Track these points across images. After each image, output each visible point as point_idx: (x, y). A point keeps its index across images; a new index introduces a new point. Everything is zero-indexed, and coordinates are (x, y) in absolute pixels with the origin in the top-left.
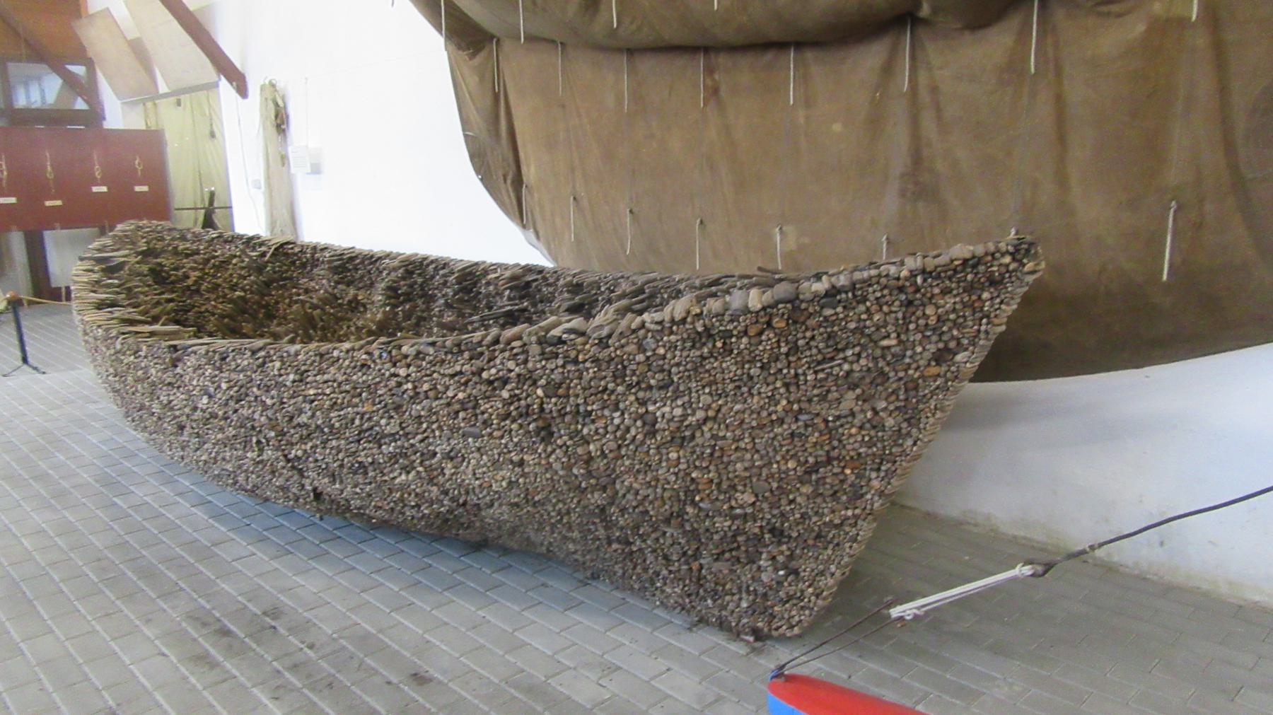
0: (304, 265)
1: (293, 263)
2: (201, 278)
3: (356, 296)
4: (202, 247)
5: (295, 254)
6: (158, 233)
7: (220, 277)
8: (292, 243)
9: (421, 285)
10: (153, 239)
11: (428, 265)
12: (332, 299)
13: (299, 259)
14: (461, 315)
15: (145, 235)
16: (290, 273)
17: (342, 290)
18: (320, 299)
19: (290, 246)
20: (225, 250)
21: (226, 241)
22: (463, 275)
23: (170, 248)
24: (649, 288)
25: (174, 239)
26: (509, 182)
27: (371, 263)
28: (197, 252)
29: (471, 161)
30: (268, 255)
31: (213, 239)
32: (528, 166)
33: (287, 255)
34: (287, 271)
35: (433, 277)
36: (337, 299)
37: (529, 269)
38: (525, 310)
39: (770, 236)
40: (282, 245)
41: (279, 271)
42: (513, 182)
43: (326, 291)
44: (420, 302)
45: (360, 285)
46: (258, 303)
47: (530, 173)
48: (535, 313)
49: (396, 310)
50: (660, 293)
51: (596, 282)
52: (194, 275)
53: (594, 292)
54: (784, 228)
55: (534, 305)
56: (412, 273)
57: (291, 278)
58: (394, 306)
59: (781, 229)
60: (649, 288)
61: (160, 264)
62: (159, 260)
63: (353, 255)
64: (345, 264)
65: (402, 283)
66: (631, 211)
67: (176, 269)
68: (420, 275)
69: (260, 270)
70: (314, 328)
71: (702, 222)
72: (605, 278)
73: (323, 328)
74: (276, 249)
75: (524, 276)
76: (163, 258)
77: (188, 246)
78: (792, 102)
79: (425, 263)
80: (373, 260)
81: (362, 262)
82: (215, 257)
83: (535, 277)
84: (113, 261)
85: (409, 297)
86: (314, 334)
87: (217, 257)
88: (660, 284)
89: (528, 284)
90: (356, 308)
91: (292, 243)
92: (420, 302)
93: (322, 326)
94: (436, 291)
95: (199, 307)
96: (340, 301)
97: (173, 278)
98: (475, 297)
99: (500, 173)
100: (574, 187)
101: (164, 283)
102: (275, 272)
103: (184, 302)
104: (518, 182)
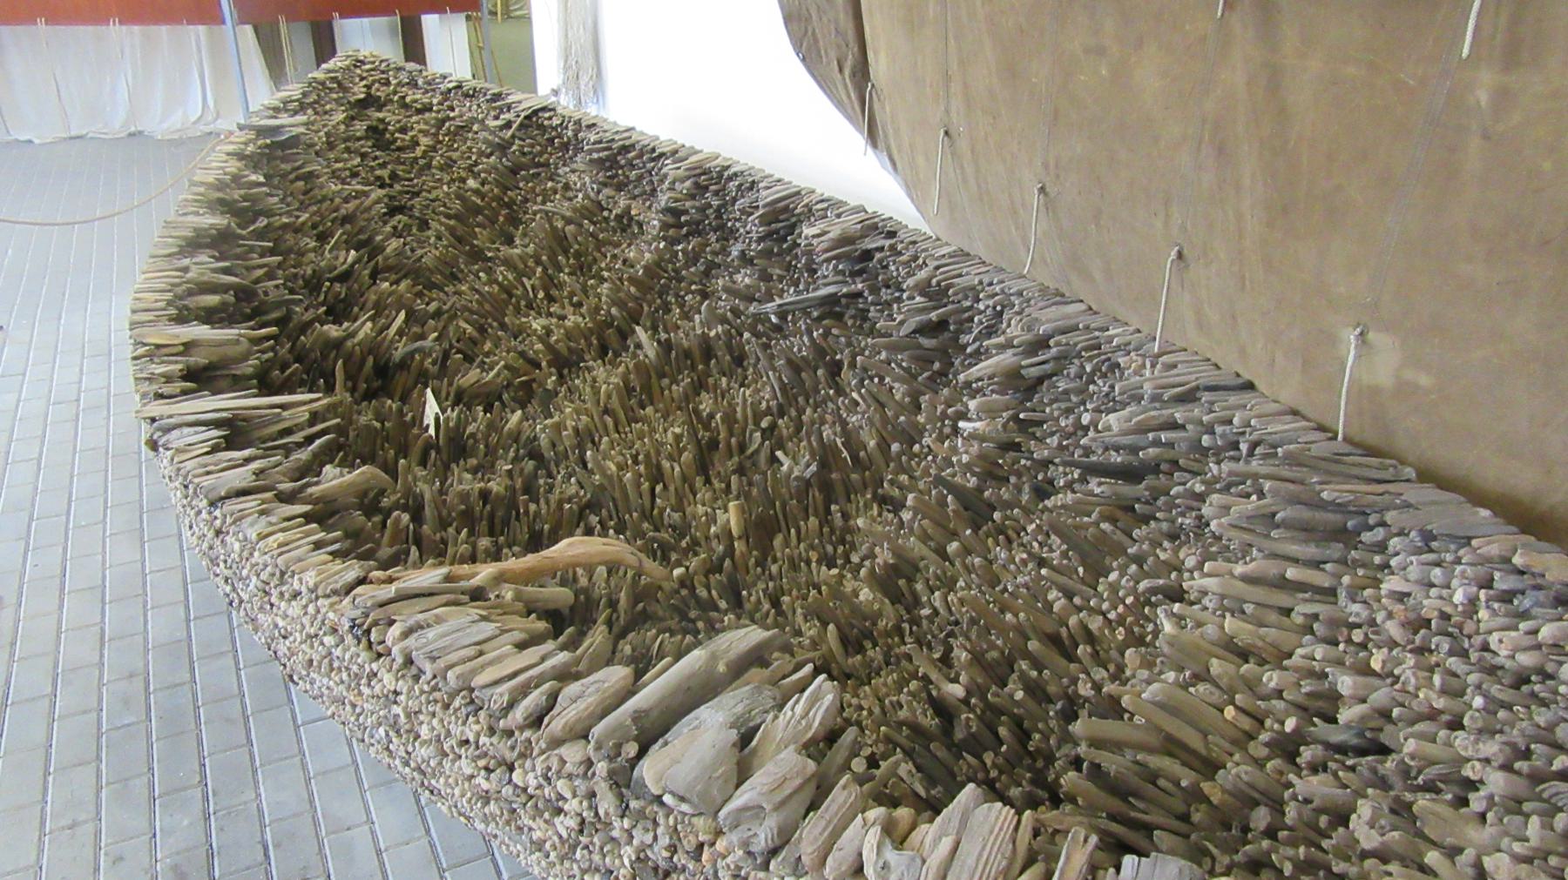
0: (565, 147)
1: (551, 141)
2: (434, 149)
3: (629, 208)
4: (435, 101)
5: (555, 129)
6: (383, 72)
7: (457, 149)
8: (550, 110)
9: (718, 210)
10: (374, 82)
11: (730, 179)
12: (595, 210)
13: (560, 136)
14: (765, 277)
15: (365, 74)
16: (546, 156)
17: (609, 197)
18: (575, 210)
19: (547, 115)
20: (464, 109)
21: (466, 95)
22: (774, 211)
23: (396, 98)
24: (1058, 344)
25: (400, 84)
26: (847, 72)
27: (653, 160)
28: (428, 108)
29: (786, 27)
30: (515, 126)
31: (449, 91)
32: (876, 53)
33: (541, 127)
34: (541, 154)
35: (734, 200)
36: (603, 209)
37: (874, 226)
38: (859, 294)
39: (1332, 340)
40: (535, 112)
41: (530, 153)
42: (853, 75)
43: (586, 196)
44: (713, 237)
45: (636, 192)
46: (499, 199)
47: (879, 66)
48: (873, 303)
49: (676, 248)
50: (1079, 356)
51: (973, 288)
52: (425, 141)
53: (967, 304)
54: (1371, 336)
55: (874, 290)
56: (706, 188)
57: (546, 165)
58: (673, 242)
59: (1361, 334)
60: (1058, 344)
61: (382, 121)
62: (381, 115)
63: (627, 143)
64: (615, 155)
65: (688, 204)
66: (1042, 190)
67: (403, 130)
68: (716, 193)
69: (503, 148)
70: (566, 252)
71: (1180, 255)
72: (991, 284)
73: (578, 255)
74: (526, 117)
75: (863, 236)
76: (389, 111)
77: (418, 96)
78: (1465, 52)
79: (726, 174)
80: (654, 155)
81: (640, 156)
82: (449, 119)
83: (879, 244)
84: (282, 134)
85: (696, 229)
86: (564, 261)
87: (453, 119)
88: (1078, 339)
89: (867, 255)
90: (629, 226)
91: (550, 110)
92: (713, 237)
93: (576, 251)
94: (738, 224)
95: (429, 192)
96: (606, 213)
97: (399, 143)
98: (790, 249)
99: (833, 55)
100: (947, 111)
101: (388, 149)
102: (524, 154)
103: (411, 180)
104: (862, 72)
